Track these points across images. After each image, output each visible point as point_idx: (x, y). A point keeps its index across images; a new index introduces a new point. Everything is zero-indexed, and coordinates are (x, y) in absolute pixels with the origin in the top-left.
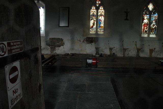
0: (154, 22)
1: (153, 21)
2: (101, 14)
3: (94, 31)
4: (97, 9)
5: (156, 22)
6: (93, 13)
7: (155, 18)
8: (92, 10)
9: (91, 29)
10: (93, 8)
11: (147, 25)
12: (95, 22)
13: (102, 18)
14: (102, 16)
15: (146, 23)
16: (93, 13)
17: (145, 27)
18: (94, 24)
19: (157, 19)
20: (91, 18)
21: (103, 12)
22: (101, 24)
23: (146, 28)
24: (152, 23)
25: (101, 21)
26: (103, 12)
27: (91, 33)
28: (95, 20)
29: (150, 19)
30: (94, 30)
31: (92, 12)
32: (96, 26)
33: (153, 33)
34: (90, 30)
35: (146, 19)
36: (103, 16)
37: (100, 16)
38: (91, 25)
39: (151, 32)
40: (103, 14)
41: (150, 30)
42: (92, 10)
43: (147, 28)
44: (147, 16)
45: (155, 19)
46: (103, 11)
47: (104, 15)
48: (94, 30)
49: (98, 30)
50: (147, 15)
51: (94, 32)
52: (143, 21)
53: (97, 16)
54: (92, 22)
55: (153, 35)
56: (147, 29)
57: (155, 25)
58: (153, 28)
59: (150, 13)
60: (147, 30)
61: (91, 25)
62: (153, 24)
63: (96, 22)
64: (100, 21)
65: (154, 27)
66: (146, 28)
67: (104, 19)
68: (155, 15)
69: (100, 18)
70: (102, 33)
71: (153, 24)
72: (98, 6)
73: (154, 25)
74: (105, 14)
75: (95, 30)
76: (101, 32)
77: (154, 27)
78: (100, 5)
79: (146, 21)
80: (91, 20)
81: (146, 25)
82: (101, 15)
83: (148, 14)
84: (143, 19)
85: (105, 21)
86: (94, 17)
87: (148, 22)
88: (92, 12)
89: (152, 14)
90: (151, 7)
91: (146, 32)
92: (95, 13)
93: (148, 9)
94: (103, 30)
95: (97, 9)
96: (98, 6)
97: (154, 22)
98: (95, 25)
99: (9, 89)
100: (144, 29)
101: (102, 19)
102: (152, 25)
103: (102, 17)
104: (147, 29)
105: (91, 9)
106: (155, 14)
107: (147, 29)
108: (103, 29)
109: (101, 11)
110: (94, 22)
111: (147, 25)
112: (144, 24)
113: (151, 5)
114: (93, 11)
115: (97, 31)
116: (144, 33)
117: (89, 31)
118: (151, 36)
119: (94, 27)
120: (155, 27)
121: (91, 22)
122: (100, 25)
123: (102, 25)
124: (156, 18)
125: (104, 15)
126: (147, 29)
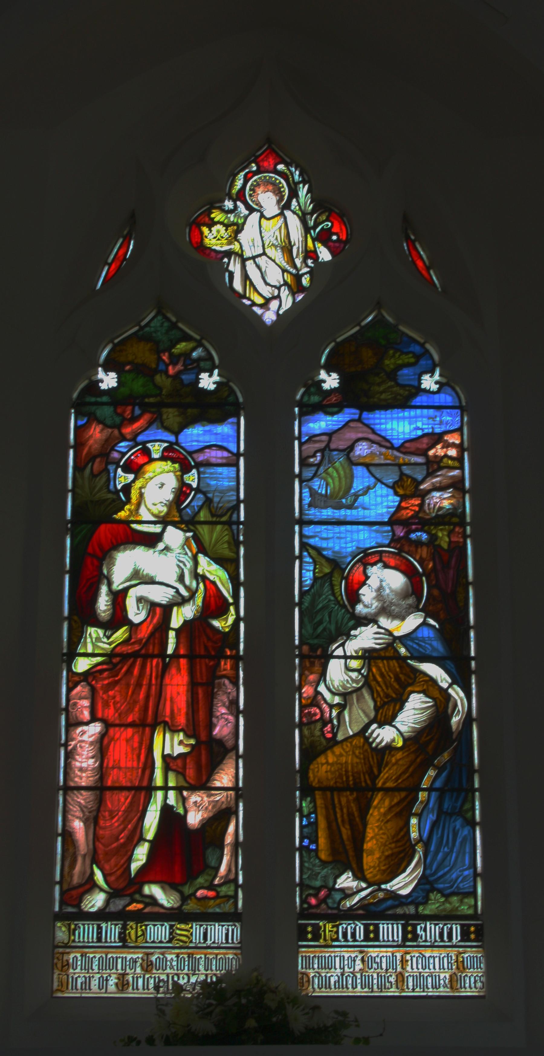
0: (395, 580)
1: (367, 558)
5: (436, 587)
7: (406, 487)
11: (203, 690)
15: (180, 616)
17: (149, 723)
19: (452, 518)
23: (169, 744)
24: (345, 634)
29: (251, 529)
33: (403, 884)
35: (178, 513)
39: (347, 855)
40: (130, 994)
41: (321, 807)
43: (205, 758)
44: (182, 460)
45: (422, 521)
50: (195, 435)
52: (90, 573)
55: (390, 930)
56: (203, 784)
57: (433, 670)
58: (385, 735)
59: (265, 374)
60: (221, 817)
62: (365, 638)
65: (414, 711)
66: (169, 744)
68: (400, 426)
71: (365, 638)
73: (389, 676)
77: (414, 711)
79: (156, 573)
81: (177, 686)
83: (212, 409)
84: (105, 527)
87: (215, 605)
89: (326, 403)
90: (265, 243)
91: (183, 852)
93: (203, 285)
97: (386, 580)
99: (368, 839)
100: (121, 791)
102: (336, 672)
104: (197, 770)
106: (406, 398)
107: (197, 770)
111: (203, 690)
112: (114, 659)
113: (268, 201)
116: (126, 886)
118: (342, 968)
120: (436, 734)
124: (442, 500)
126: (224, 778)
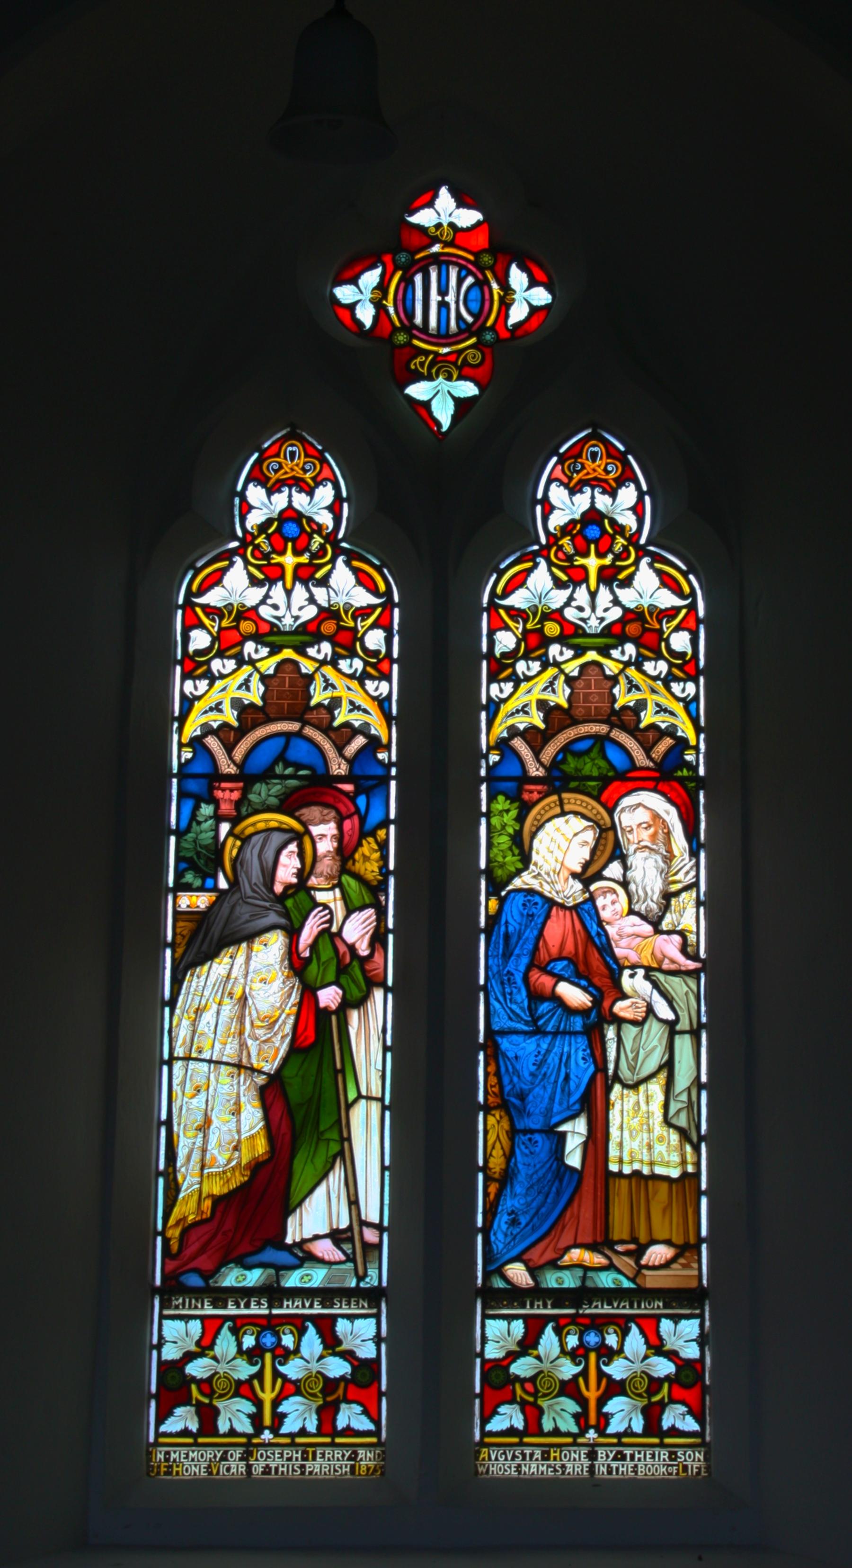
2: (591, 705)
3: (329, 1395)
4: (440, 522)
6: (288, 695)
8: (236, 586)
9: (173, 1289)
10: (262, 505)
12: (370, 1037)
13: (609, 847)
14: (631, 779)
16: (288, 695)
18: (300, 1105)
20: (203, 862)
21: (347, 643)
22: (594, 1105)
25: (600, 967)
26: (347, 643)
27: (193, 1464)
28: (357, 930)
30: (308, 1356)
31: (239, 629)
32: (399, 1170)
34: (176, 1334)
36: (668, 776)
37: (558, 781)
38: (211, 1124)
40: (671, 706)
42: (236, 586)
46: (646, 589)
47: (698, 759)
48: (308, 1356)
49: (498, 1334)
51: (299, 1414)
53: (439, 787)
54: (229, 1012)
61: (211, 1124)
63: (380, 1005)
64: (574, 995)
67: (713, 905)
69: (561, 844)
70: (667, 1157)
72: (444, 413)
74: (722, 722)
75: (361, 1333)
76: (606, 1399)
78: (536, 393)
80: (207, 939)
82: (588, 763)
85: (738, 974)
86: (325, 834)
88: (534, 644)
92: (358, 700)
94: (684, 1335)
95: (440, 522)
96: (444, 413)
98: (368, 1133)
101: (631, 876)
103: (643, 810)
105: (209, 531)
108: (683, 1300)
109: (601, 590)
110: (318, 1038)
114: (277, 605)
115: (431, 1376)
117: (116, 1381)
119: (315, 1216)
121: (180, 1028)
122: (576, 1131)
123: (644, 1134)
125: (698, 759)
